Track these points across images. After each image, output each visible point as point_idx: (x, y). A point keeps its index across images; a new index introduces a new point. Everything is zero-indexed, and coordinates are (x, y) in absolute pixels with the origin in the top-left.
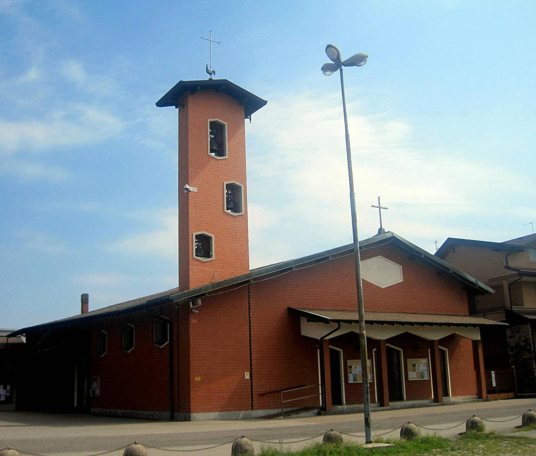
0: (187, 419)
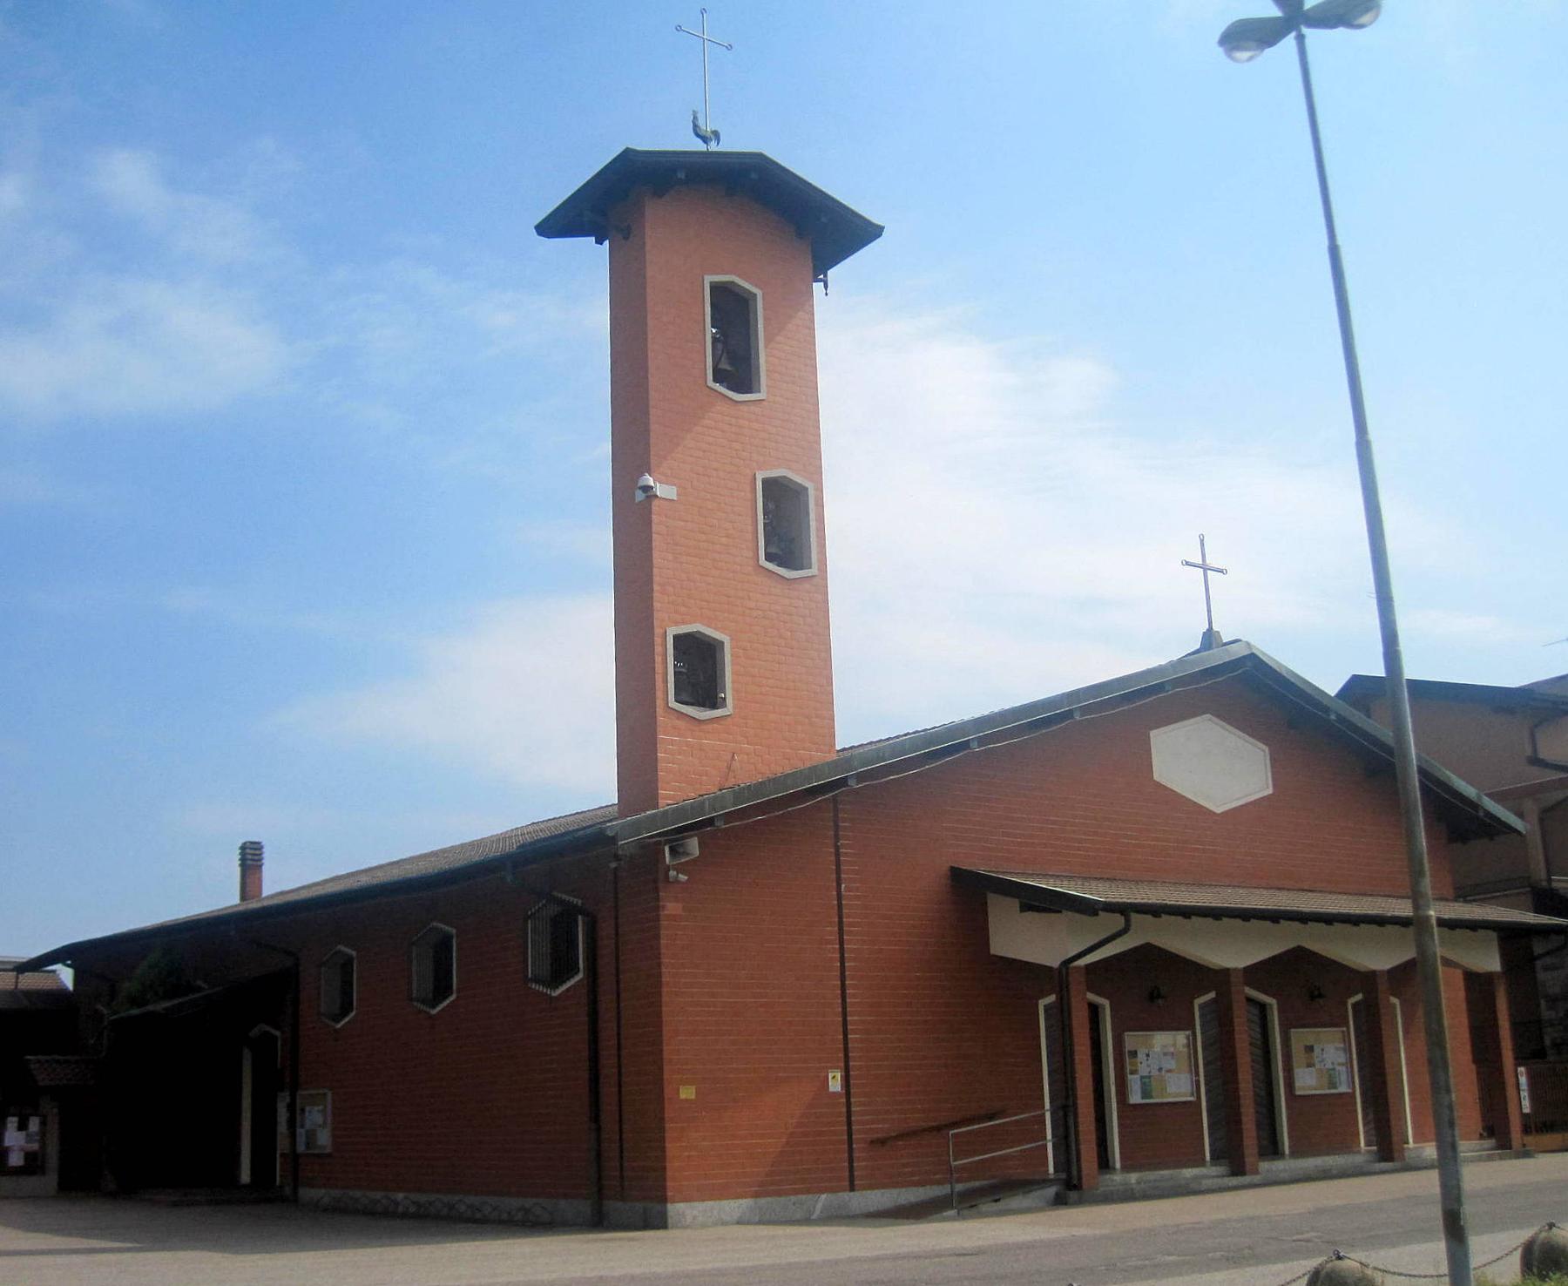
0: (654, 1220)
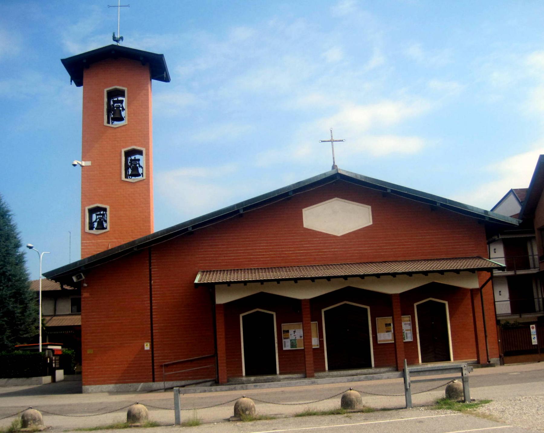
0: (79, 391)
